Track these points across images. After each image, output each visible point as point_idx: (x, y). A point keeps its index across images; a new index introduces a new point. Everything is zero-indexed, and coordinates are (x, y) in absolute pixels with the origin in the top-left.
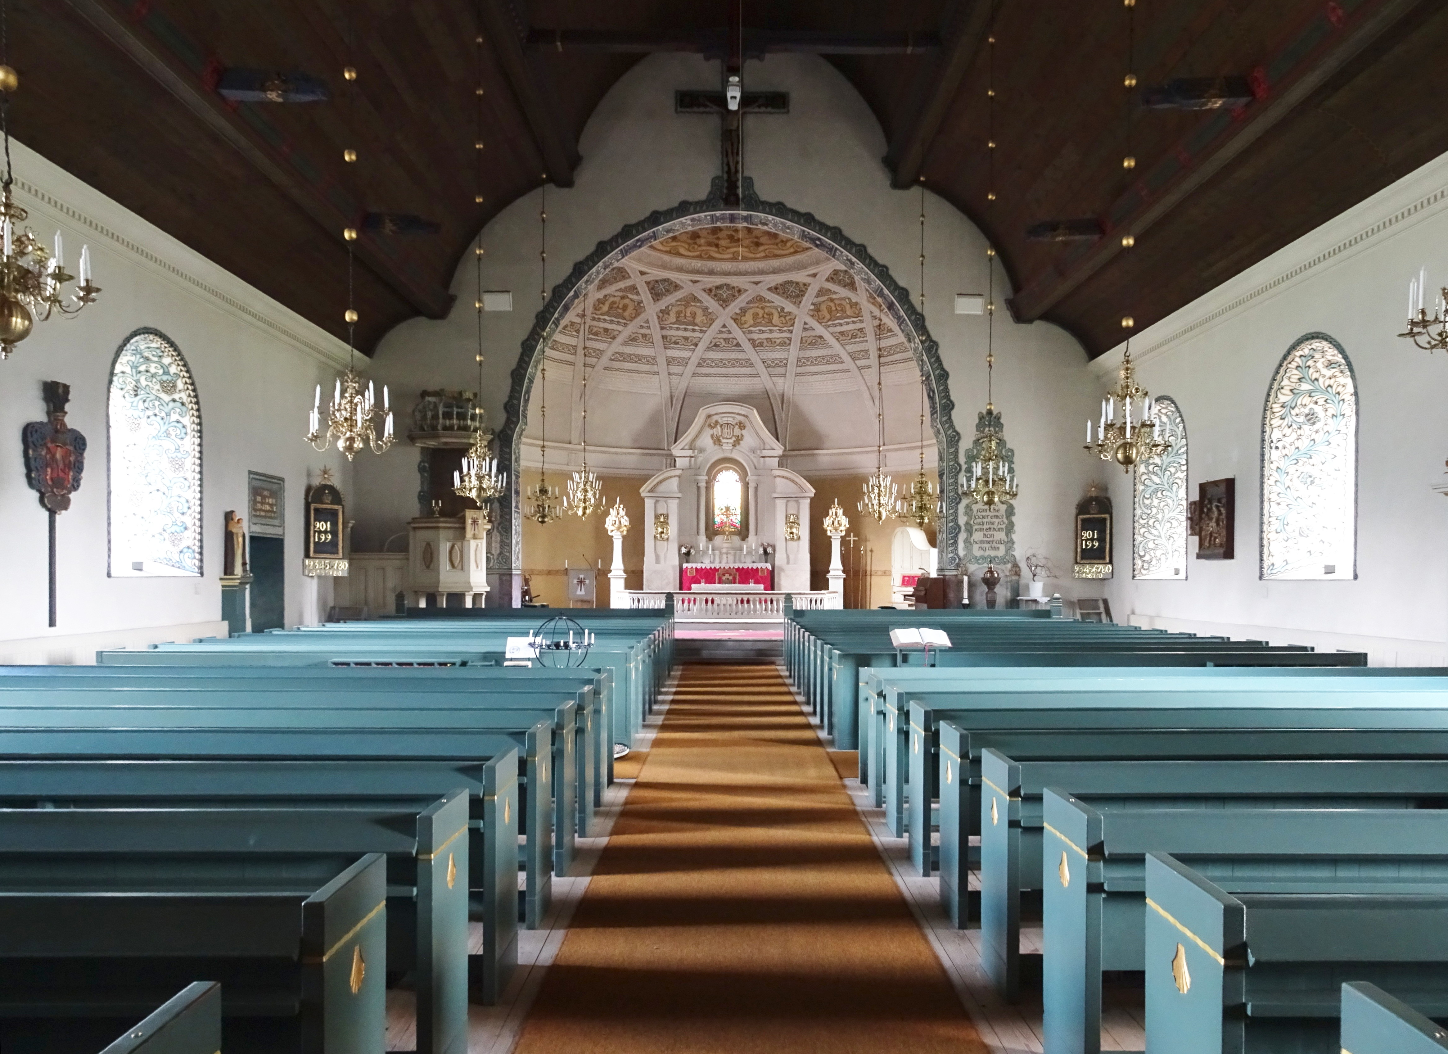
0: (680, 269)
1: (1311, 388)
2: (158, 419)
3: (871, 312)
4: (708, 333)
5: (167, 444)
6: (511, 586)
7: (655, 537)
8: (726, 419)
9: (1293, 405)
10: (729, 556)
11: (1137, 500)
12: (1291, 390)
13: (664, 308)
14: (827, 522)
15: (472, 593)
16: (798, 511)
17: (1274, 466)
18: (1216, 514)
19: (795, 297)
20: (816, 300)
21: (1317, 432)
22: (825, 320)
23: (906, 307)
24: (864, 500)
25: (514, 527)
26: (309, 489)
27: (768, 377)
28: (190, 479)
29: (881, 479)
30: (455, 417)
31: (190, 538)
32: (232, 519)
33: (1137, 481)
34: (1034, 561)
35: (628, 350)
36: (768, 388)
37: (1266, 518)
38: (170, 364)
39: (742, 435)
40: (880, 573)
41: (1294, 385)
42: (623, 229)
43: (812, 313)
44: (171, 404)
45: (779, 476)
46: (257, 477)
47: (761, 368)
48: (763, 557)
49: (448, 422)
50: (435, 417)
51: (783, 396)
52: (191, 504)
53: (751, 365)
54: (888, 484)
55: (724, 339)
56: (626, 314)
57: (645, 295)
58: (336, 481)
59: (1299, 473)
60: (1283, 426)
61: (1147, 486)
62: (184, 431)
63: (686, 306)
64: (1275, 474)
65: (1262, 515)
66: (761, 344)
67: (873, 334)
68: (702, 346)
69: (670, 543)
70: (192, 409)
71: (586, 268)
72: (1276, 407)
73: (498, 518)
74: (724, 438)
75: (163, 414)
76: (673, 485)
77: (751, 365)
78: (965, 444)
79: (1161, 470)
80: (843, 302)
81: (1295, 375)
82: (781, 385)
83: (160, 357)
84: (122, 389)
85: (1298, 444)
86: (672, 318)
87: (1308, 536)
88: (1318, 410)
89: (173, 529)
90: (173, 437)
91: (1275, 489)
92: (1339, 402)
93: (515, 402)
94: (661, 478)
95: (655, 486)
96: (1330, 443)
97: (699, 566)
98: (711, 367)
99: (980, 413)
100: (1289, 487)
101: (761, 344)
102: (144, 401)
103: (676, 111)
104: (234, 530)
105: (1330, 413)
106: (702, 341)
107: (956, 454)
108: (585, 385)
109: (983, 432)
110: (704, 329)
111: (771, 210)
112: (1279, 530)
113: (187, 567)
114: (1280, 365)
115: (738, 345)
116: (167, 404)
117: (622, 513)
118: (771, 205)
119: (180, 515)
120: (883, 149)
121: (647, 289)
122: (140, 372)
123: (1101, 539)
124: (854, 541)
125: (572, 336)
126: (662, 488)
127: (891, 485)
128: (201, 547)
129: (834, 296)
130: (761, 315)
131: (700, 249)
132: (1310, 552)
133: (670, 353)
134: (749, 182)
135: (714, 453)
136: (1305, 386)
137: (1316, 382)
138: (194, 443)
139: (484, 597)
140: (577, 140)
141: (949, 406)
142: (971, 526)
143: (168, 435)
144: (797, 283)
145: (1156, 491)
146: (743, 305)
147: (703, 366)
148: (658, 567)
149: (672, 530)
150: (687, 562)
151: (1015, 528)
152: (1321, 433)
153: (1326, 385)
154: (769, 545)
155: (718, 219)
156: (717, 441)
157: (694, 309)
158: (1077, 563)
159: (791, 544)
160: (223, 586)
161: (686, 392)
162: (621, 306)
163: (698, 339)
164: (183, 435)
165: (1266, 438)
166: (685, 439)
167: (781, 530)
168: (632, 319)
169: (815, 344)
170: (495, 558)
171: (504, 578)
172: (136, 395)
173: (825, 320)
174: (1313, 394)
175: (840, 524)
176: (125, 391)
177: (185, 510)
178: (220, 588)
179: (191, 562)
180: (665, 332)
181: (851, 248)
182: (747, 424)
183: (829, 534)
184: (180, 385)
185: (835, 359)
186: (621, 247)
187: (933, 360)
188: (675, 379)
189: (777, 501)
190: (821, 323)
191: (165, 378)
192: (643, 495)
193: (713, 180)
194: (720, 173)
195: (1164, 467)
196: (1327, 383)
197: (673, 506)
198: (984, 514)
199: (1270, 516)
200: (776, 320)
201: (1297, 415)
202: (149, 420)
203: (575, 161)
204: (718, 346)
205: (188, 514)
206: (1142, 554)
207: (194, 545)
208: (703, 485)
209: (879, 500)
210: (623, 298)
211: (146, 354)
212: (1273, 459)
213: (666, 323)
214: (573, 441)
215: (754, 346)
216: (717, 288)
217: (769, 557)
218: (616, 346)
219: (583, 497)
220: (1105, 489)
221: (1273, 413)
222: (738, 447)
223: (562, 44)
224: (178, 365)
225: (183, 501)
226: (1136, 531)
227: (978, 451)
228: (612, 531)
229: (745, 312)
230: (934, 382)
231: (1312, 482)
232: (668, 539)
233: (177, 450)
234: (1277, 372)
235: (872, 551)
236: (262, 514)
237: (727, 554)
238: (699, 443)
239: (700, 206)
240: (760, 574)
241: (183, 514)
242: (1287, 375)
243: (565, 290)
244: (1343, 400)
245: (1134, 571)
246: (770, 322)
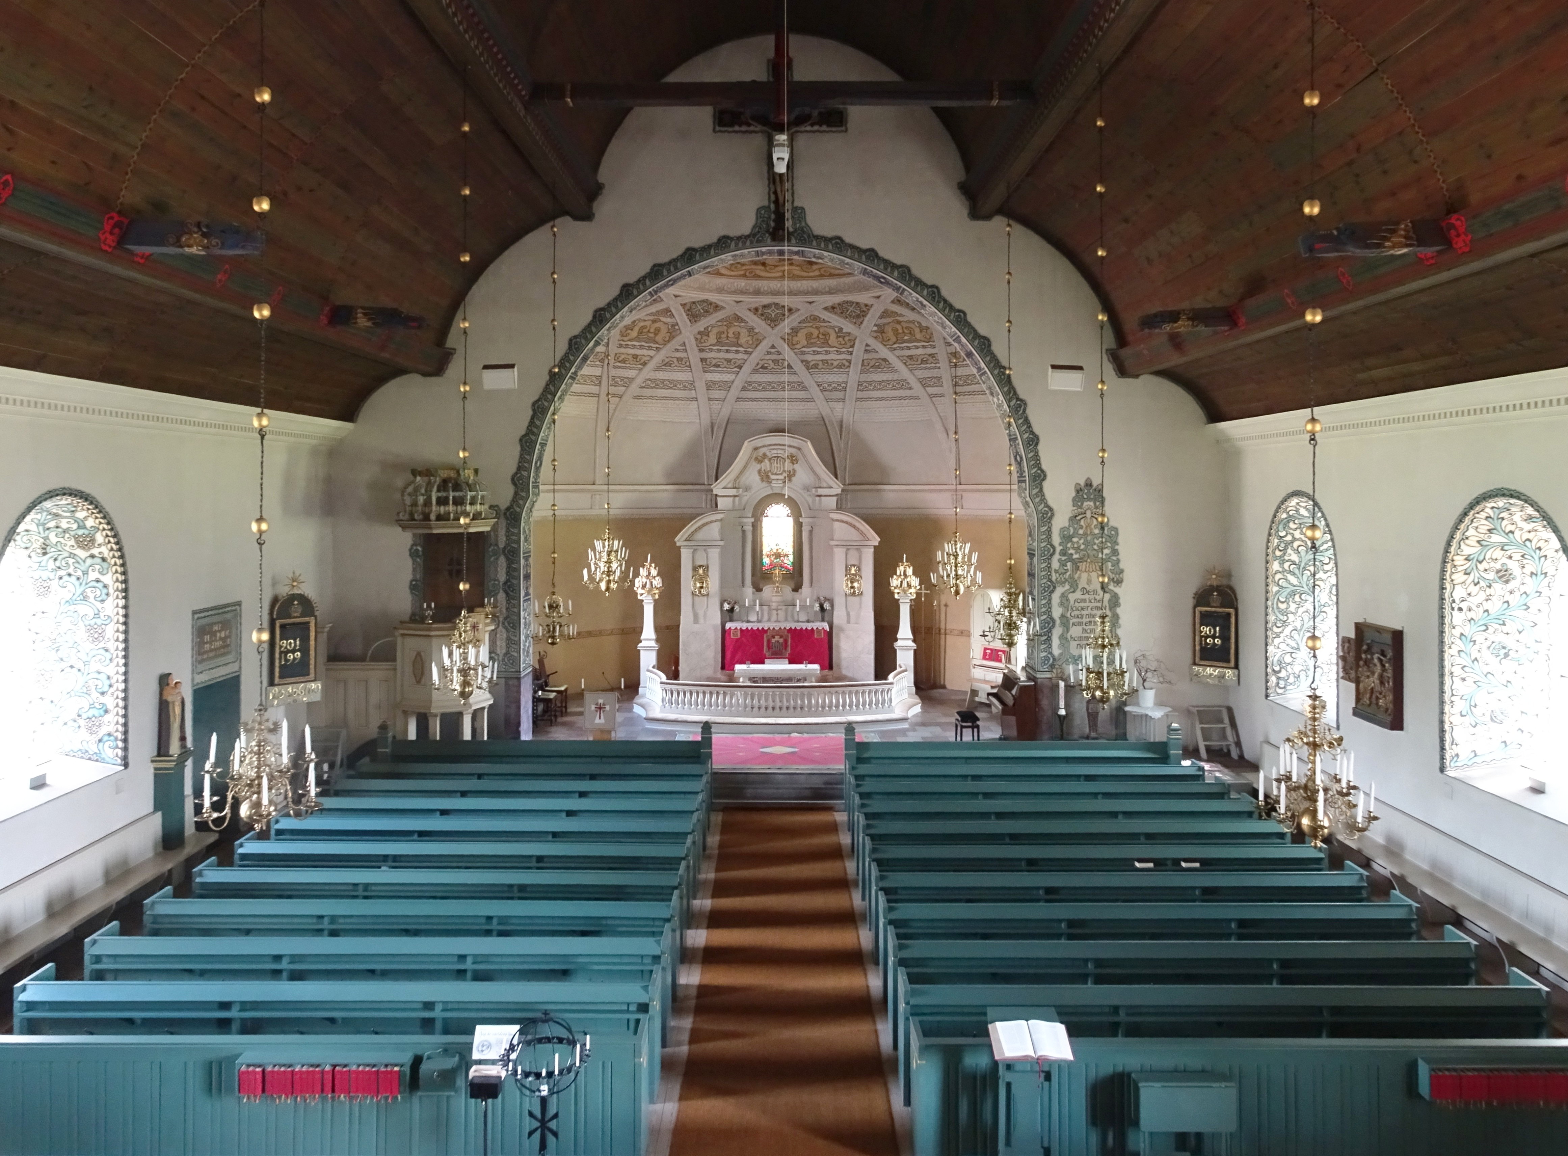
0: (720, 290)
1: (1505, 540)
2: (73, 579)
3: (944, 338)
4: (753, 355)
5: (84, 609)
6: (519, 692)
7: (693, 594)
8: (775, 451)
9: (1481, 558)
10: (779, 612)
11: (1269, 603)
12: (1478, 542)
13: (702, 329)
14: (895, 582)
15: (471, 711)
17: (1457, 632)
18: (1378, 669)
19: (854, 318)
20: (880, 322)
21: (1511, 593)
22: (890, 343)
23: (988, 359)
24: (937, 571)
25: (522, 621)
26: (275, 600)
27: (825, 403)
28: (112, 650)
30: (451, 502)
31: (112, 723)
32: (168, 684)
33: (1270, 580)
34: (1143, 664)
35: (661, 375)
36: (824, 414)
37: (1447, 697)
38: (86, 518)
39: (794, 471)
41: (1482, 536)
42: (652, 269)
43: (875, 335)
44: (89, 561)
45: (837, 520)
46: (202, 615)
47: (815, 392)
48: (820, 615)
49: (442, 509)
50: (428, 503)
51: (841, 422)
52: (113, 681)
53: (805, 389)
54: (967, 551)
55: (773, 361)
56: (659, 338)
57: (681, 317)
58: (308, 589)
59: (1489, 643)
60: (1468, 582)
61: (1282, 587)
62: (105, 591)
63: (729, 326)
64: (1458, 641)
65: (1442, 692)
66: (816, 366)
67: (947, 362)
68: (747, 369)
70: (115, 564)
71: (608, 315)
72: (1459, 560)
73: (504, 611)
74: (773, 474)
75: (79, 573)
76: (714, 531)
77: (805, 389)
78: (1060, 522)
79: (1299, 569)
80: (911, 325)
81: (1484, 526)
82: (837, 411)
83: (73, 511)
84: (26, 548)
85: (1487, 605)
86: (712, 339)
87: (1501, 723)
88: (1513, 566)
89: (90, 714)
90: (92, 599)
91: (1458, 660)
92: (1540, 558)
93: (525, 473)
95: (693, 533)
96: (1529, 608)
97: (744, 626)
98: (758, 390)
99: (1077, 484)
100: (1476, 659)
101: (816, 366)
102: (55, 560)
103: (714, 131)
104: (169, 699)
105: (1528, 569)
106: (747, 363)
107: (1049, 532)
109: (1080, 507)
110: (750, 350)
111: (826, 246)
112: (1464, 713)
113: (107, 759)
114: (1465, 514)
115: (790, 367)
116: (84, 561)
117: (654, 572)
118: (827, 240)
119: (99, 695)
120: (960, 175)
121: (682, 311)
122: (48, 529)
123: (1225, 638)
124: (925, 594)
125: (597, 366)
126: (700, 536)
128: (126, 733)
129: (901, 319)
130: (815, 335)
131: (744, 268)
132: (1505, 742)
133: (710, 377)
134: (799, 213)
135: (760, 490)
136: (1496, 538)
137: (1511, 535)
138: (117, 606)
139: (486, 710)
140: (596, 165)
141: (1039, 476)
142: (1068, 620)
143: (85, 598)
144: (857, 303)
145: (1293, 594)
146: (795, 324)
147: (749, 390)
149: (713, 583)
150: (731, 620)
151: (1120, 621)
152: (1517, 594)
153: (1524, 539)
154: (826, 599)
155: (763, 253)
156: (765, 477)
157: (738, 329)
158: (1195, 664)
159: (851, 599)
160: (156, 769)
162: (652, 330)
163: (742, 361)
164: (104, 597)
165: (1447, 596)
166: (727, 478)
167: (841, 584)
168: (666, 342)
169: (879, 367)
170: (501, 659)
171: (511, 682)
172: (45, 554)
173: (890, 343)
174: (1506, 548)
175: (909, 586)
176: (31, 549)
177: (106, 688)
178: (152, 771)
179: (112, 752)
180: (704, 355)
181: (922, 290)
182: (800, 456)
183: (896, 596)
184: (100, 538)
185: (903, 384)
186: (650, 290)
187: (1020, 421)
188: (716, 405)
189: (836, 550)
190: (885, 345)
191: (80, 532)
192: (678, 544)
193: (758, 210)
194: (766, 203)
195: (1303, 565)
196: (1526, 536)
197: (714, 558)
198: (1082, 605)
199: (1453, 695)
200: (833, 339)
201: (1486, 570)
202: (61, 581)
203: (594, 191)
204: (766, 368)
205: (109, 693)
206: (1277, 668)
207: (117, 731)
208: (749, 528)
209: (956, 571)
210: (654, 321)
211: (55, 511)
212: (1455, 623)
213: (704, 344)
214: (597, 482)
215: (808, 368)
216: (765, 307)
217: (826, 614)
218: (648, 372)
219: (606, 569)
220: (1229, 576)
221: (1455, 566)
223: (572, 100)
224: (96, 518)
225: (103, 677)
226: (1270, 641)
227: (1075, 529)
228: (642, 595)
229: (797, 332)
230: (1021, 446)
231: (1506, 655)
232: (708, 595)
233: (97, 615)
234: (1461, 521)
236: (211, 655)
237: (777, 610)
238: (744, 480)
239: (741, 241)
240: (816, 636)
241: (103, 693)
242: (1474, 525)
243: (583, 341)
244: (1546, 556)
245: (1267, 689)
246: (826, 343)
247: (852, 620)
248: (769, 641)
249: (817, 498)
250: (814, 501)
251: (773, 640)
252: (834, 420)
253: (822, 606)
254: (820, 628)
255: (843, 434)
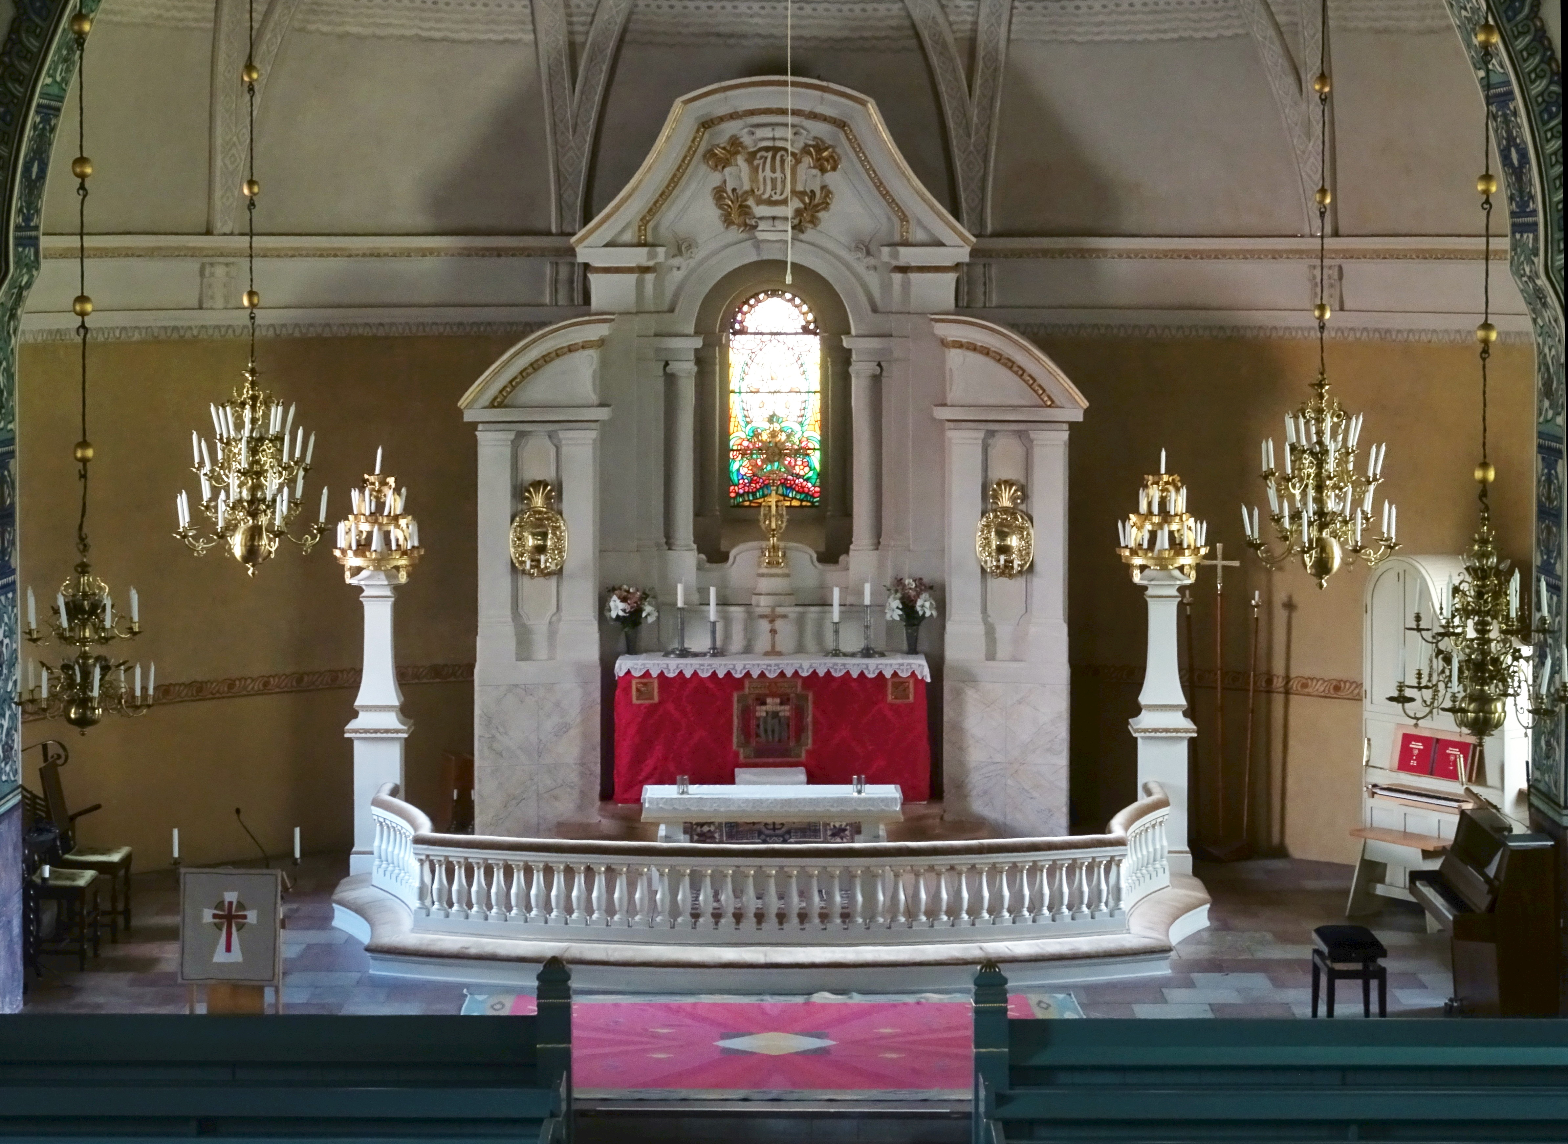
8: (767, 133)
10: (779, 624)
16: (1028, 466)
29: (1327, 425)
36: (918, 15)
40: (1320, 687)
45: (959, 345)
48: (902, 634)
51: (972, 42)
69: (567, 586)
74: (760, 202)
94: (534, 354)
95: (513, 384)
97: (672, 666)
108: (250, 67)
117: (394, 502)
127: (1365, 443)
148: (527, 671)
154: (922, 586)
161: (625, 31)
182: (844, 148)
192: (469, 416)
208: (686, 368)
209: (1319, 501)
222: (810, 234)
230: (1523, 119)
235: (1290, 606)
247: (1003, 649)
248: (747, 714)
249: (897, 277)
250: (886, 287)
251: (761, 711)
252: (950, 39)
253: (908, 606)
254: (904, 674)
255: (978, 81)
